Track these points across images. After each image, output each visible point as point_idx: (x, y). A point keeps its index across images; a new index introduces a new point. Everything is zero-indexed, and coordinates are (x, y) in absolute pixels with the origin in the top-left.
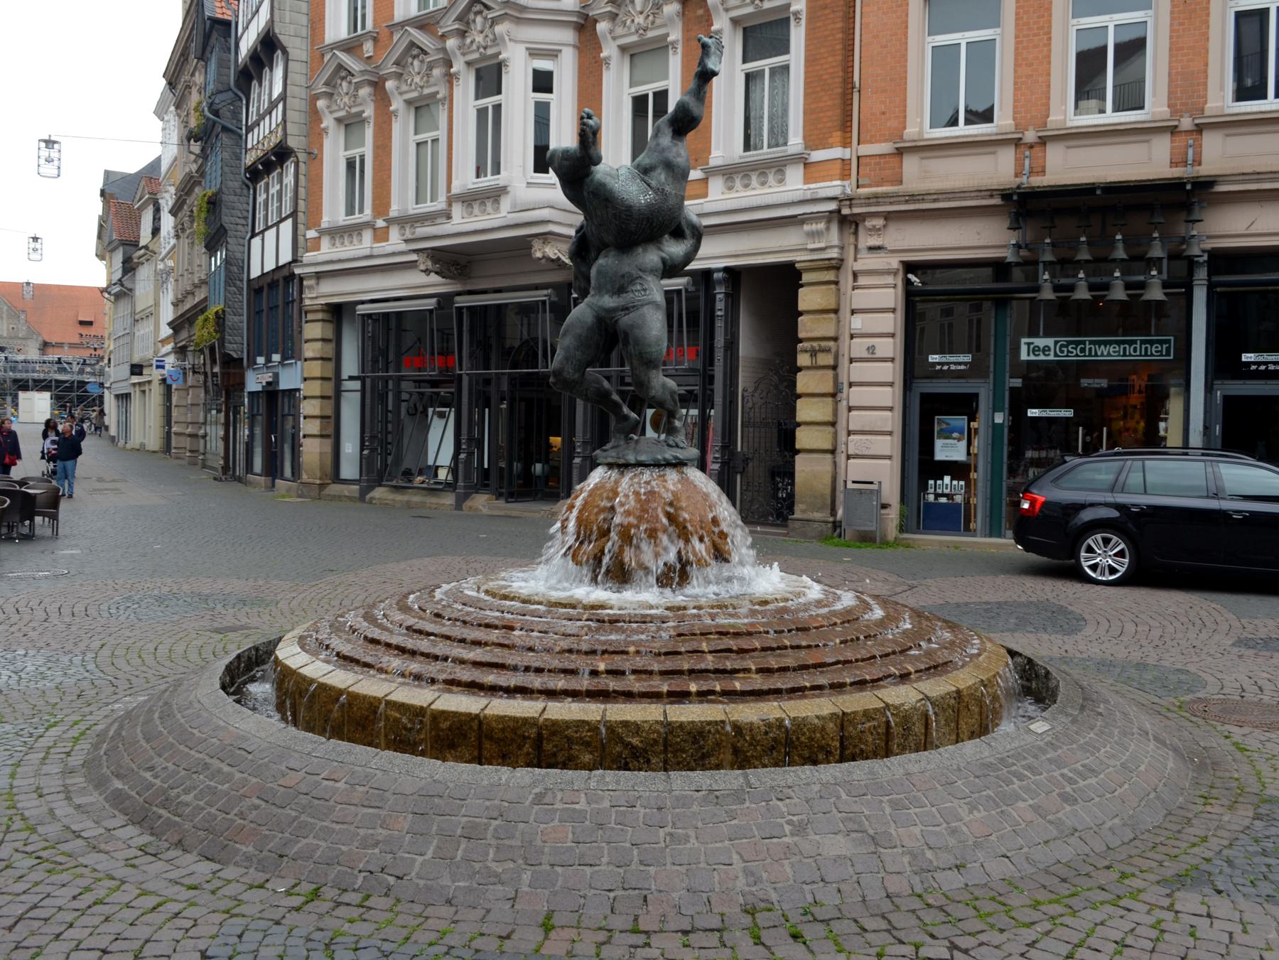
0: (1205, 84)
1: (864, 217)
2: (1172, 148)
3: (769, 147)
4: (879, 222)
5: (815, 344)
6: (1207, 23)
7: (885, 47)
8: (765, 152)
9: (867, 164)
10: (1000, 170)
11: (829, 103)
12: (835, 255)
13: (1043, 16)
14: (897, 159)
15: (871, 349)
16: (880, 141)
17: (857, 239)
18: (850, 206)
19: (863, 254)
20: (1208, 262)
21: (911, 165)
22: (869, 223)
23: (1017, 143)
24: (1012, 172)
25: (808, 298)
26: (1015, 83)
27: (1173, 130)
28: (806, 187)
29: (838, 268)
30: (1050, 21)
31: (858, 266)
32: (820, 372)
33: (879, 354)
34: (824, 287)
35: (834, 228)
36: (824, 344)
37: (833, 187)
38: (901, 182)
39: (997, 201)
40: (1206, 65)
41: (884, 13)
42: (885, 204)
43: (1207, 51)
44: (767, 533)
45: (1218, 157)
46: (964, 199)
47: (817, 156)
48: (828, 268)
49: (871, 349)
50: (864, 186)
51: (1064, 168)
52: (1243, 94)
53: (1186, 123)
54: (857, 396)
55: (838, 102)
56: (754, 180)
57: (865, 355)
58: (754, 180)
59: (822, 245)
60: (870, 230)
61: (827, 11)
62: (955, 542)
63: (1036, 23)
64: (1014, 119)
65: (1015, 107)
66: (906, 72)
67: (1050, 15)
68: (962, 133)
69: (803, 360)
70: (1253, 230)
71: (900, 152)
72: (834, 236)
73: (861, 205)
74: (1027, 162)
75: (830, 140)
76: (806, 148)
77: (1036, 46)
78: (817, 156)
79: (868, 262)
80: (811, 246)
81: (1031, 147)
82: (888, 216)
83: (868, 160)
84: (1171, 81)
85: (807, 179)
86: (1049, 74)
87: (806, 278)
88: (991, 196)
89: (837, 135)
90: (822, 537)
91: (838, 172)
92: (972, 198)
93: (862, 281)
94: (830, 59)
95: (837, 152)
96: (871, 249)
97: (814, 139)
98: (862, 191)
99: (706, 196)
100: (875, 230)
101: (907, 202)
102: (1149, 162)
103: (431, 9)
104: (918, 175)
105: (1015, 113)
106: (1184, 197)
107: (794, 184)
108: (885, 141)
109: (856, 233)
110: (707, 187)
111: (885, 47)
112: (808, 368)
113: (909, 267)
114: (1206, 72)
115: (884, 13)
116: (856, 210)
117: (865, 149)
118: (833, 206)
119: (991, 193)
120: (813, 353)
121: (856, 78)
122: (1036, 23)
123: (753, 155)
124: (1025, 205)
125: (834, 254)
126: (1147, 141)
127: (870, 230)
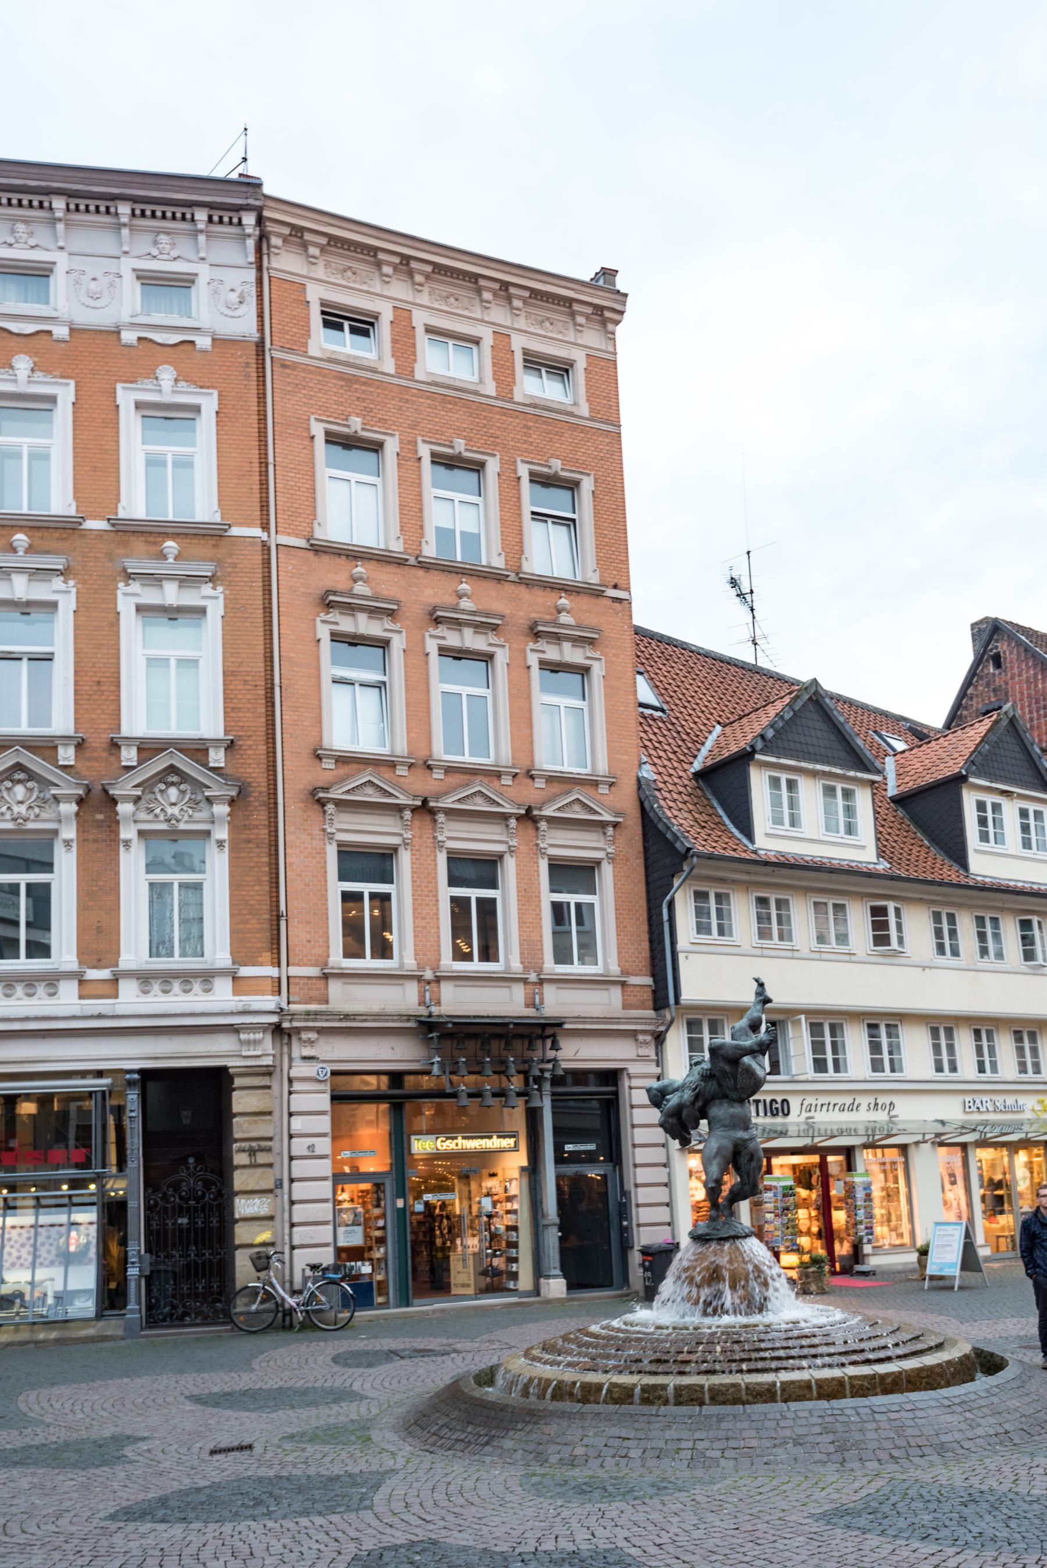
0: (542, 950)
1: (298, 1030)
2: (526, 994)
3: (181, 956)
4: (313, 1036)
5: (254, 1144)
6: (539, 906)
7: (308, 885)
8: (177, 962)
9: (296, 984)
10: (405, 999)
11: (258, 926)
12: (271, 1063)
13: (431, 882)
14: (323, 982)
15: (311, 1147)
16: (306, 965)
17: (290, 1050)
18: (291, 1021)
19: (297, 1062)
20: (552, 1079)
21: (335, 988)
22: (304, 1036)
23: (419, 979)
24: (417, 1002)
25: (241, 1101)
26: (415, 931)
27: (525, 981)
28: (237, 998)
29: (270, 1074)
30: (436, 887)
31: (294, 1073)
32: (260, 1170)
33: (318, 1152)
34: (260, 1091)
35: (269, 1038)
36: (263, 1144)
37: (269, 1002)
38: (327, 1002)
39: (412, 1024)
40: (541, 936)
41: (305, 857)
42: (321, 1020)
43: (541, 927)
44: (219, 1331)
45: (556, 1003)
46: (387, 1021)
47: (245, 971)
48: (264, 1074)
49: (311, 1147)
50: (294, 1003)
51: (457, 1002)
52: (348, 954)
53: (533, 977)
54: (300, 1190)
55: (267, 926)
56: (176, 986)
57: (306, 1153)
58: (176, 986)
59: (259, 1053)
60: (305, 1042)
61: (251, 845)
62: (382, 1315)
63: (426, 887)
64: (522, 963)
65: (415, 950)
66: (327, 909)
67: (436, 883)
68: (575, 971)
69: (240, 1159)
70: (580, 1056)
71: (326, 977)
72: (268, 1044)
73: (300, 1020)
74: (428, 994)
75: (260, 959)
76: (234, 963)
77: (428, 905)
78: (245, 971)
79: (301, 1070)
80: (244, 1053)
81: (429, 983)
82: (320, 1031)
83: (297, 980)
84: (521, 945)
85: (236, 992)
86: (438, 928)
87: (238, 1082)
88: (408, 1020)
89: (267, 956)
90: (269, 1328)
91: (270, 988)
92: (393, 1021)
93: (296, 1086)
94: (257, 888)
95: (272, 971)
96: (304, 1058)
97: (241, 954)
98: (293, 1007)
99: (116, 997)
100: (311, 1043)
101: (340, 1020)
102: (507, 1003)
103: (329, 670)
104: (342, 997)
105: (416, 954)
106: (548, 1031)
107: (222, 997)
108: (311, 965)
109: (289, 1044)
110: (117, 990)
111: (308, 885)
112: (244, 1167)
113: (334, 1073)
114: (541, 941)
115: (305, 857)
116: (296, 1024)
117: (294, 971)
118: (274, 1019)
119: (409, 1018)
120: (252, 1152)
121: (283, 907)
122: (426, 887)
123: (161, 963)
124: (430, 1029)
125: (268, 1061)
126: (401, 985)
127: (305, 1042)
